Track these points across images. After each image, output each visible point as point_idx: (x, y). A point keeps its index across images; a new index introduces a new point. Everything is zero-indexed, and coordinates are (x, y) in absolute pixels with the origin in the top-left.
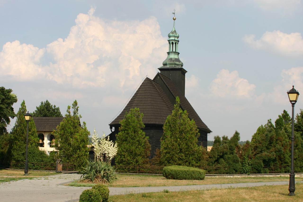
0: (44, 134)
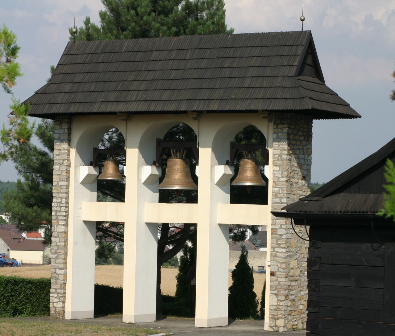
0: (193, 125)
